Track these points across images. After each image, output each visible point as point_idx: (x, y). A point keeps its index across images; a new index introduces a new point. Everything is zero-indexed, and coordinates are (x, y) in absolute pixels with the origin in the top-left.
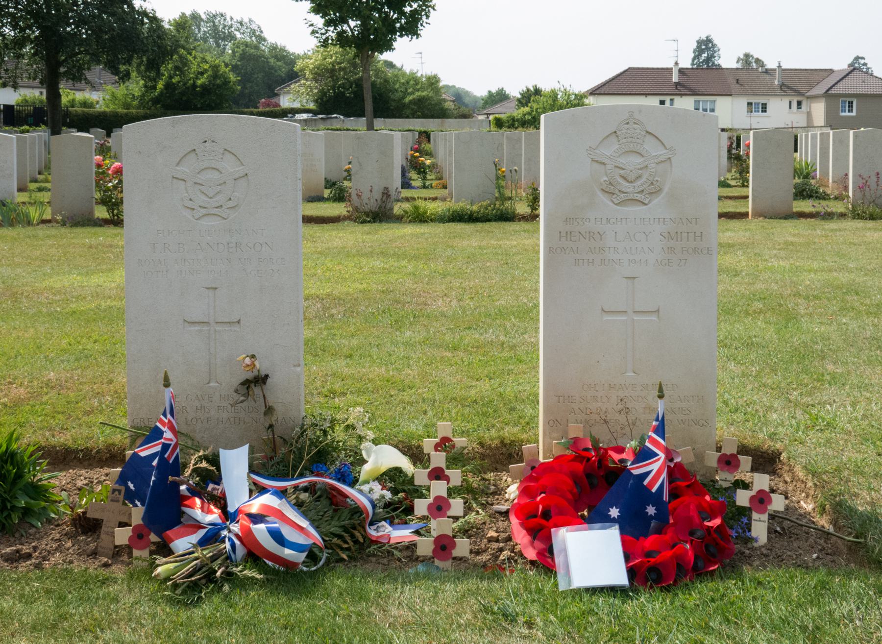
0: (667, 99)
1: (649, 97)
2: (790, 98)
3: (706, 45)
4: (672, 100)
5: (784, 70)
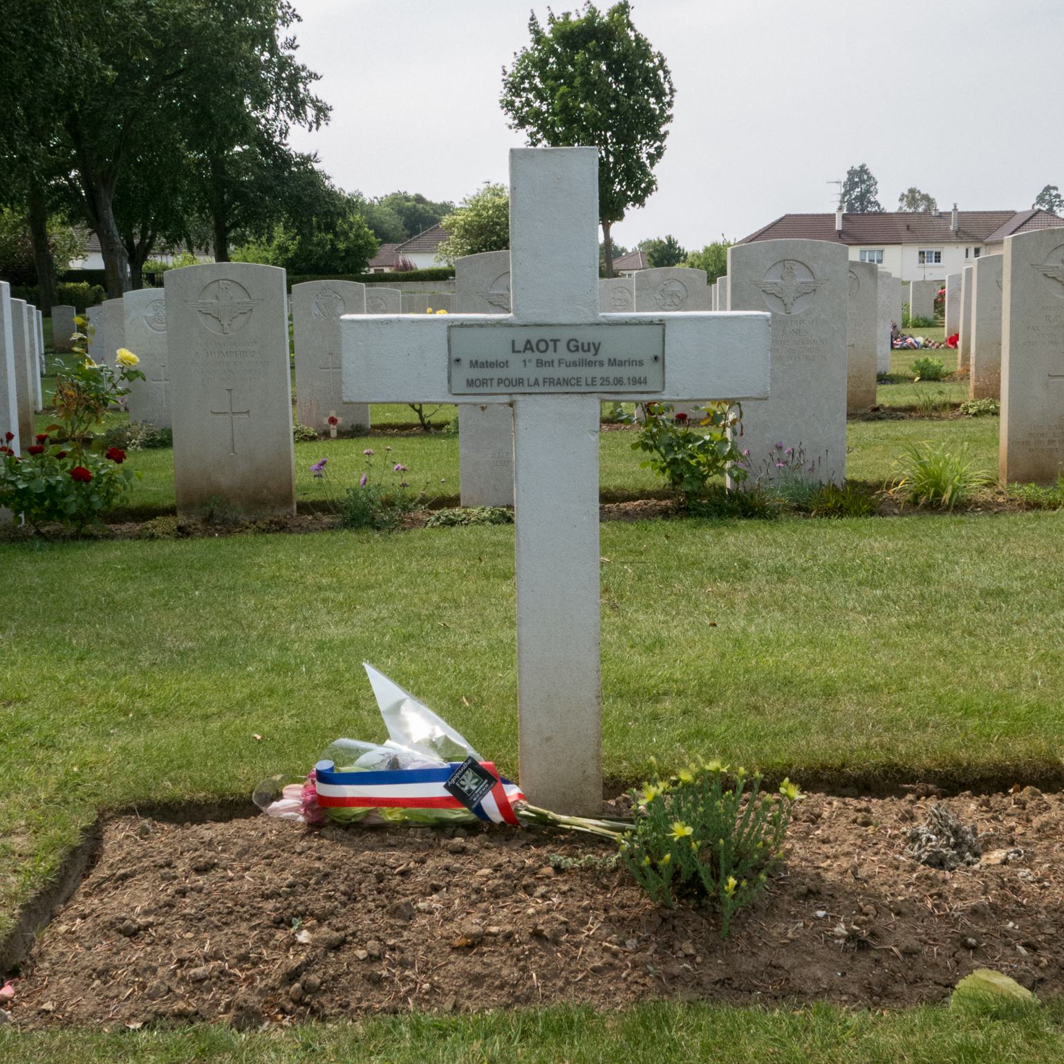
2: (968, 246)
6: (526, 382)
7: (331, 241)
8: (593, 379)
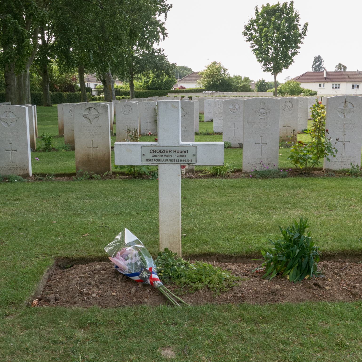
0: (322, 84)
3: (318, 59)
4: (324, 84)
7: (163, 79)
8: (178, 160)
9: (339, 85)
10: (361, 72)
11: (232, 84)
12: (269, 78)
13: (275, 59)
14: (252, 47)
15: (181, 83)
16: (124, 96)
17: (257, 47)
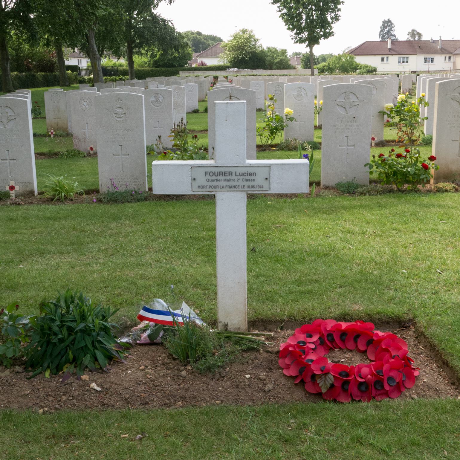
0: (385, 57)
1: (376, 56)
2: (445, 55)
4: (387, 57)
5: (443, 41)
6: (219, 187)
7: (172, 54)
9: (407, 58)
10: (458, 40)
11: (265, 59)
12: (303, 49)
13: (311, 26)
14: (280, 11)
15: (201, 57)
16: (121, 77)
17: (285, 11)
